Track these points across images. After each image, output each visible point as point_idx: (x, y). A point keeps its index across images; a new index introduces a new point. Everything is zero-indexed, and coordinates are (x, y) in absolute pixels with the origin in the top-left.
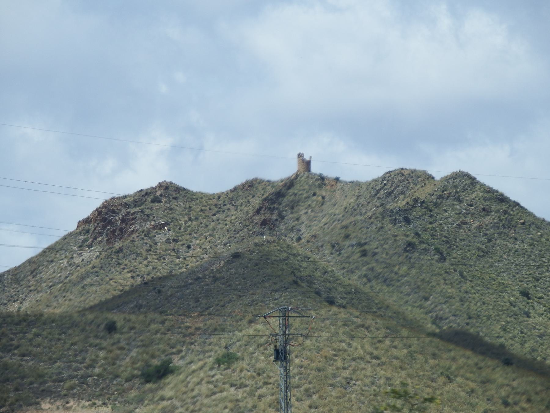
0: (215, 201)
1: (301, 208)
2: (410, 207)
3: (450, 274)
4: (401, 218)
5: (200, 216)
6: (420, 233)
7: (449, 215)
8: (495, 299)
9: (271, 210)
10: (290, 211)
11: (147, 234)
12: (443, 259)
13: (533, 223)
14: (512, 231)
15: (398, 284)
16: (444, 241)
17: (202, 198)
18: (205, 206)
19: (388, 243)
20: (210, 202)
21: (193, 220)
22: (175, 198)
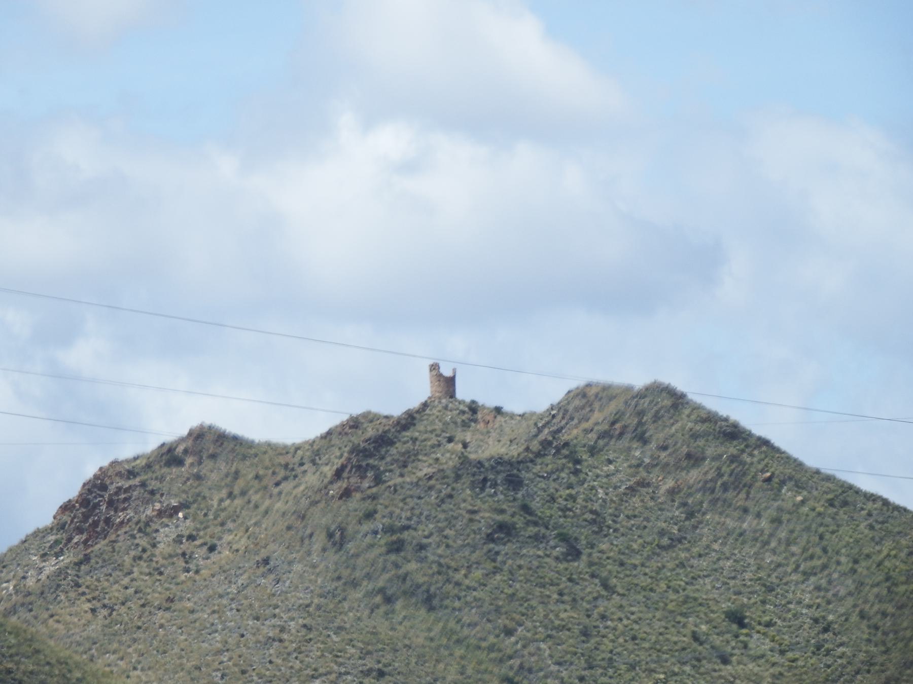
0: (282, 460)
1: (420, 465)
3: (578, 584)
7: (615, 469)
8: (662, 630)
9: (361, 470)
11: (145, 527)
12: (574, 553)
13: (791, 478)
14: (742, 495)
15: (457, 604)
16: (586, 520)
17: (265, 453)
19: (454, 526)
22: (213, 456)
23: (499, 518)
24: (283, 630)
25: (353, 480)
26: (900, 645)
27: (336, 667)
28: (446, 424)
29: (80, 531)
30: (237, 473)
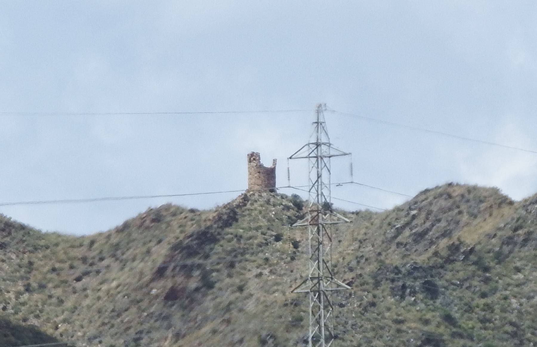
0: (77, 253)
1: (249, 266)
2: (440, 261)
4: (418, 284)
5: (49, 282)
6: (457, 315)
9: (187, 270)
10: (226, 272)
16: (506, 332)
17: (57, 245)
18: (62, 261)
19: (381, 337)
20: (74, 253)
21: (34, 290)
23: (426, 328)
30: (31, 263)
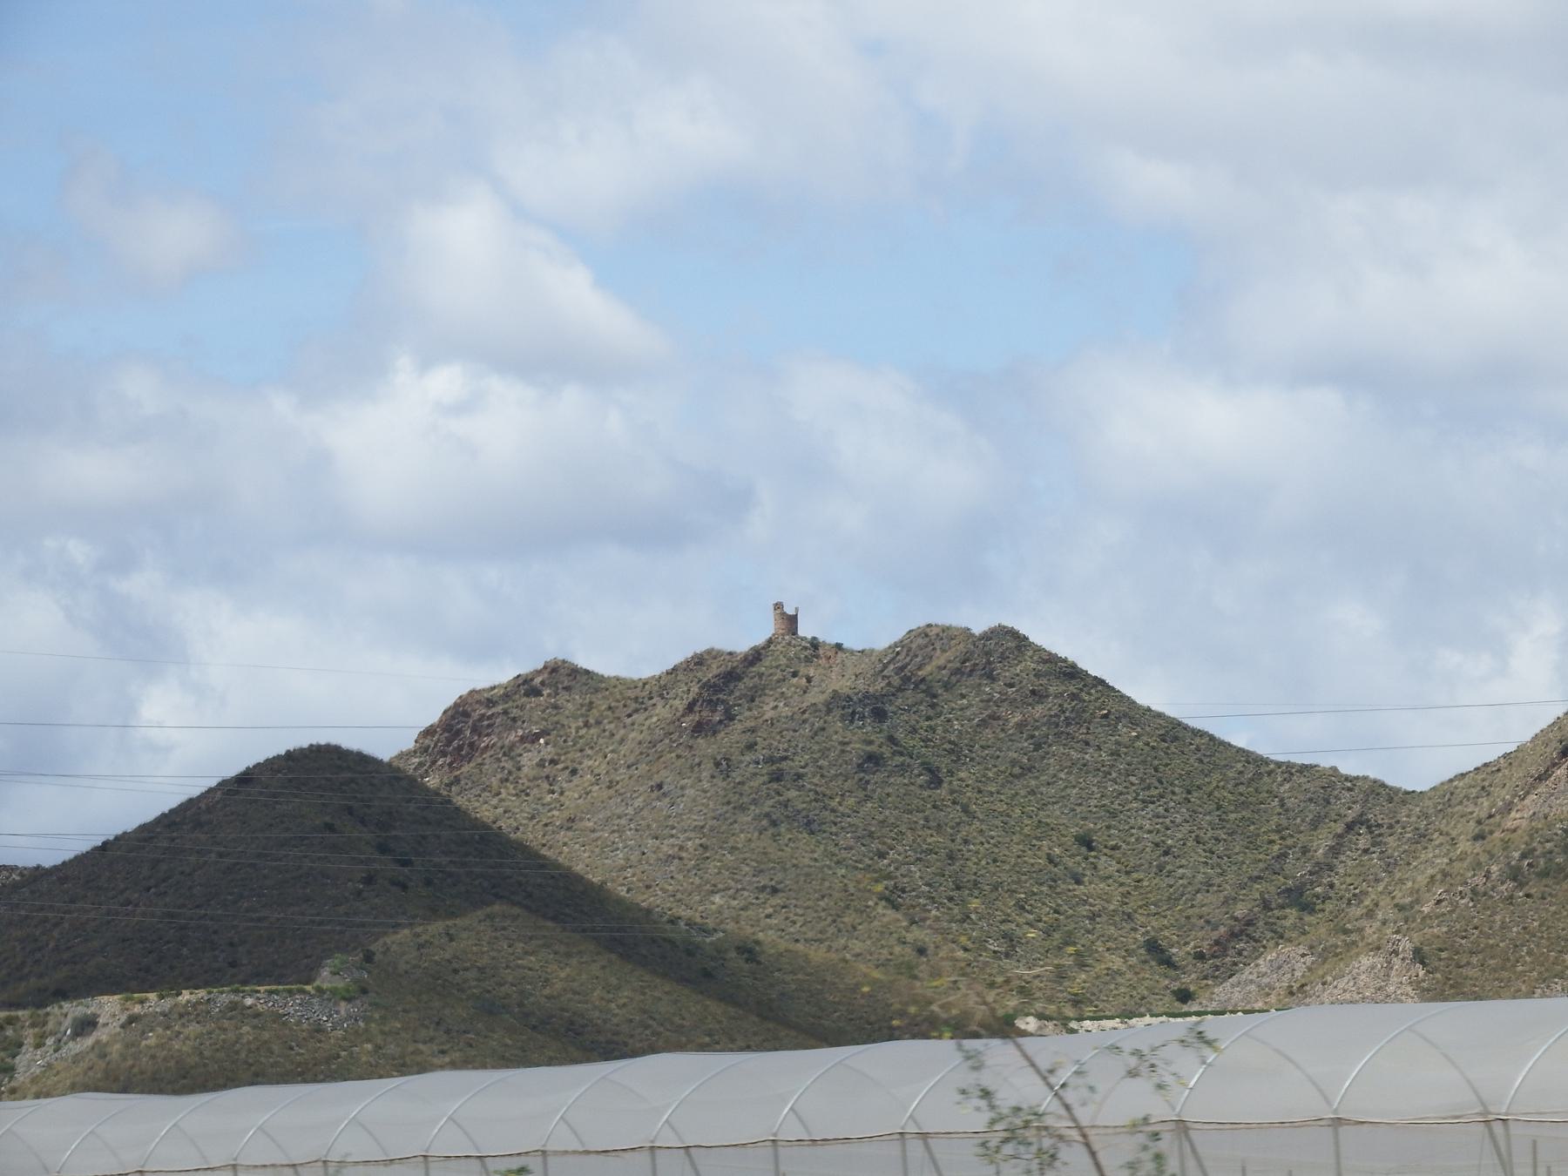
1: (767, 699)
9: (712, 704)
11: (509, 752)
12: (936, 782)
15: (834, 829)
22: (567, 689)
23: (868, 748)
24: (681, 848)
25: (704, 714)
26: (1234, 868)
27: (732, 884)
28: (790, 659)
29: (444, 754)
